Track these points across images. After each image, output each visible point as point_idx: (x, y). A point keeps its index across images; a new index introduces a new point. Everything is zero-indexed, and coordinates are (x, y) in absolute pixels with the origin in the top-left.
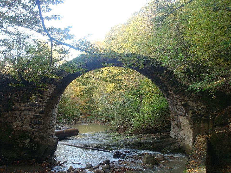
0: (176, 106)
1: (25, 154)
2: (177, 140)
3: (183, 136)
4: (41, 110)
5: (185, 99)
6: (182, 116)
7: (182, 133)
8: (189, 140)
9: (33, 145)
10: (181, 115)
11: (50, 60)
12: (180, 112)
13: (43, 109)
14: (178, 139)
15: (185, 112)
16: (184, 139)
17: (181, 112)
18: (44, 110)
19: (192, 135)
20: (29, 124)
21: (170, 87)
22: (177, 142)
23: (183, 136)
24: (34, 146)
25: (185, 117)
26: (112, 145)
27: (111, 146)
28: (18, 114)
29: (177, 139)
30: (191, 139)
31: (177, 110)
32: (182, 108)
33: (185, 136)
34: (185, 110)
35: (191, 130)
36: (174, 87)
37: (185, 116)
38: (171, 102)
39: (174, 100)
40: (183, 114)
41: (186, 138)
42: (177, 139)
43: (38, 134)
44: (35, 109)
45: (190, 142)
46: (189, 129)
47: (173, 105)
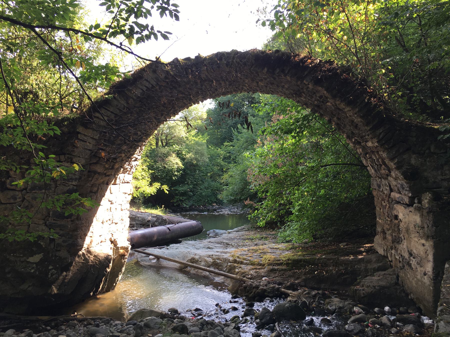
0: (387, 179)
1: (30, 289)
2: (392, 261)
3: (406, 255)
4: (69, 187)
5: (413, 161)
6: (403, 204)
7: (404, 246)
8: (422, 269)
9: (50, 267)
10: (400, 203)
11: (74, 73)
12: (397, 195)
13: (74, 185)
14: (394, 259)
15: (410, 195)
16: (409, 265)
17: (400, 195)
18: (75, 188)
19: (431, 257)
20: (44, 220)
21: (369, 130)
22: (391, 267)
23: (406, 255)
24: (52, 269)
25: (411, 209)
26: (245, 261)
27: (242, 263)
28: (20, 198)
29: (390, 259)
30: (429, 267)
31: (391, 190)
32: (402, 185)
33: (412, 258)
34: (411, 189)
35: (429, 244)
36: (381, 131)
37: (412, 206)
38: (375, 171)
39: (381, 165)
40: (406, 200)
41: (413, 262)
42: (390, 259)
43: (64, 241)
44: (56, 187)
45: (425, 274)
46: (423, 241)
47: (380, 178)
